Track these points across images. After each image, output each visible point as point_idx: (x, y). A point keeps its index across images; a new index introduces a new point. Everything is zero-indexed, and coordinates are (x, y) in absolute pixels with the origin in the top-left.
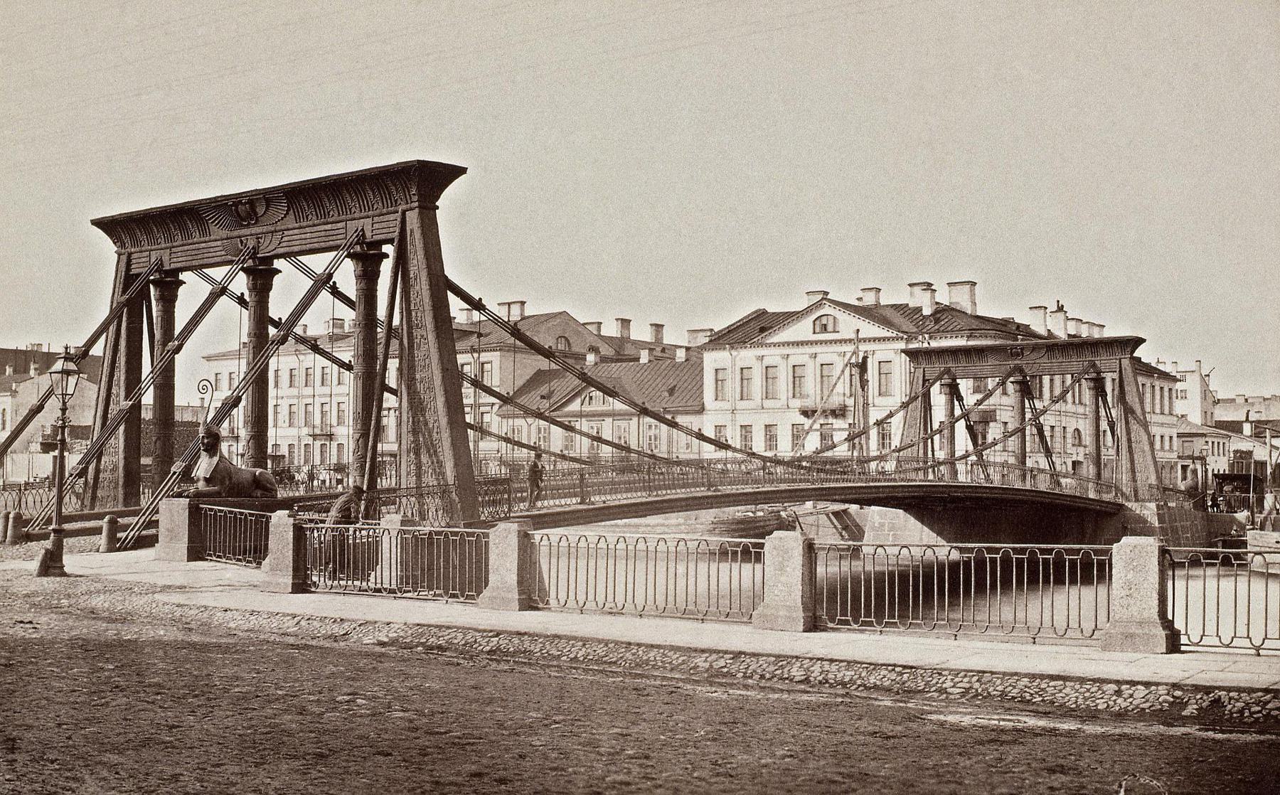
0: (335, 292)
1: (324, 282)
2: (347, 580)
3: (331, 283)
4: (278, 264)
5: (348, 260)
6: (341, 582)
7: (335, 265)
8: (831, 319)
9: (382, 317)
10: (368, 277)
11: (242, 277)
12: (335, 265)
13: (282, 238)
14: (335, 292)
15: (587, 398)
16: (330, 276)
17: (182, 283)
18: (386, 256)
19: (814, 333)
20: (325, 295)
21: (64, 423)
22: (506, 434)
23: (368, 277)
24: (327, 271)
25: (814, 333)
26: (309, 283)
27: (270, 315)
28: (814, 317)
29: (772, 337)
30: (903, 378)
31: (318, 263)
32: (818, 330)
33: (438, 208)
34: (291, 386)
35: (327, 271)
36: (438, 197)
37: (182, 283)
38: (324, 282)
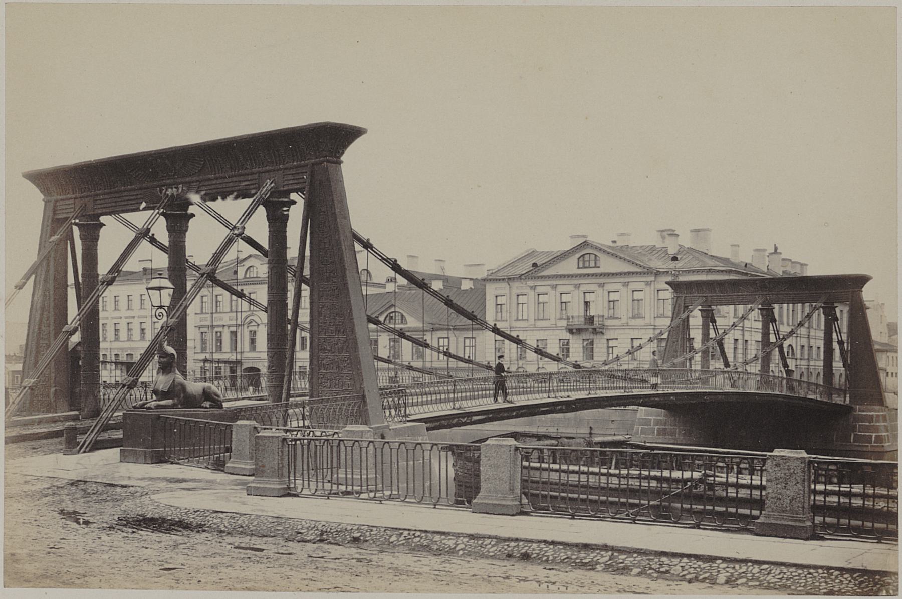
0: (153, 240)
1: (144, 234)
2: (347, 485)
3: (150, 234)
4: (103, 219)
5: (162, 218)
6: (340, 487)
7: (151, 221)
8: (593, 257)
9: (293, 258)
10: (278, 223)
11: (162, 220)
12: (151, 221)
13: (198, 188)
14: (153, 240)
15: (388, 318)
16: (148, 230)
17: (102, 225)
18: (294, 202)
19: (578, 268)
20: (145, 244)
21: (286, 411)
22: (469, 357)
23: (278, 223)
24: (145, 227)
25: (578, 268)
26: (132, 235)
27: (167, 255)
28: (578, 255)
29: (543, 271)
30: (652, 303)
31: (139, 218)
32: (581, 265)
33: (342, 162)
34: (128, 309)
35: (145, 227)
36: (343, 153)
37: (102, 225)
38: (144, 234)
